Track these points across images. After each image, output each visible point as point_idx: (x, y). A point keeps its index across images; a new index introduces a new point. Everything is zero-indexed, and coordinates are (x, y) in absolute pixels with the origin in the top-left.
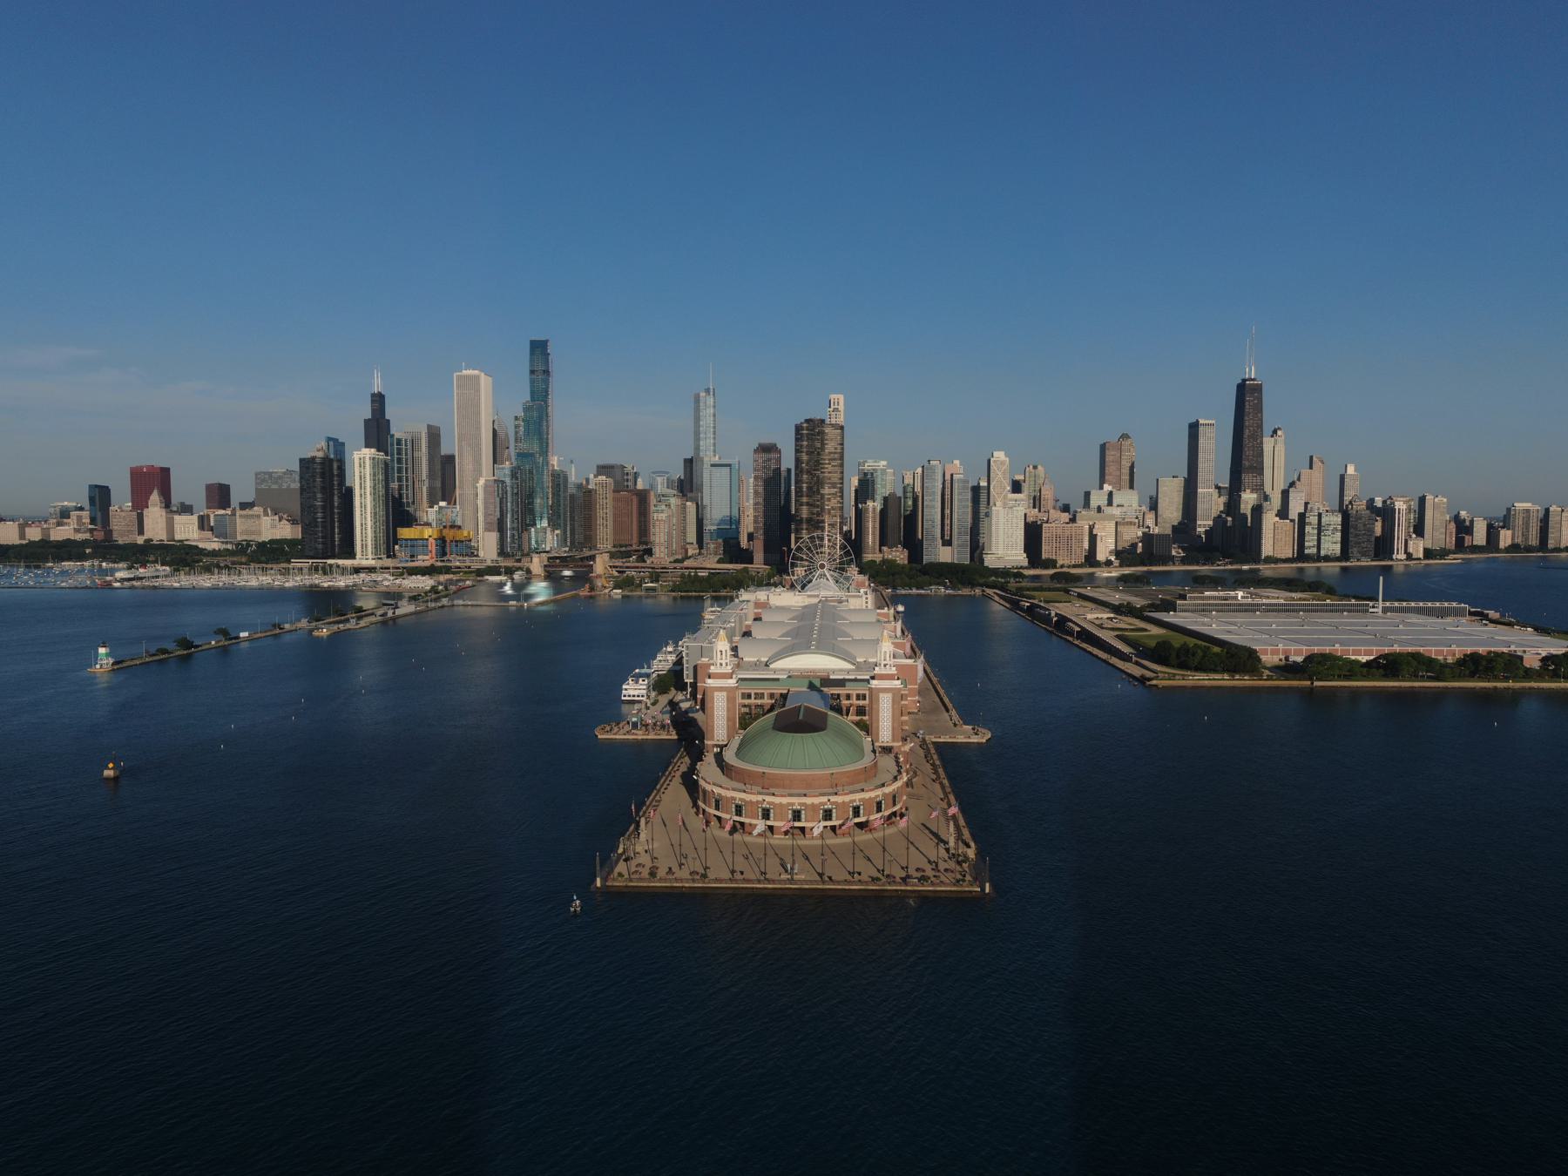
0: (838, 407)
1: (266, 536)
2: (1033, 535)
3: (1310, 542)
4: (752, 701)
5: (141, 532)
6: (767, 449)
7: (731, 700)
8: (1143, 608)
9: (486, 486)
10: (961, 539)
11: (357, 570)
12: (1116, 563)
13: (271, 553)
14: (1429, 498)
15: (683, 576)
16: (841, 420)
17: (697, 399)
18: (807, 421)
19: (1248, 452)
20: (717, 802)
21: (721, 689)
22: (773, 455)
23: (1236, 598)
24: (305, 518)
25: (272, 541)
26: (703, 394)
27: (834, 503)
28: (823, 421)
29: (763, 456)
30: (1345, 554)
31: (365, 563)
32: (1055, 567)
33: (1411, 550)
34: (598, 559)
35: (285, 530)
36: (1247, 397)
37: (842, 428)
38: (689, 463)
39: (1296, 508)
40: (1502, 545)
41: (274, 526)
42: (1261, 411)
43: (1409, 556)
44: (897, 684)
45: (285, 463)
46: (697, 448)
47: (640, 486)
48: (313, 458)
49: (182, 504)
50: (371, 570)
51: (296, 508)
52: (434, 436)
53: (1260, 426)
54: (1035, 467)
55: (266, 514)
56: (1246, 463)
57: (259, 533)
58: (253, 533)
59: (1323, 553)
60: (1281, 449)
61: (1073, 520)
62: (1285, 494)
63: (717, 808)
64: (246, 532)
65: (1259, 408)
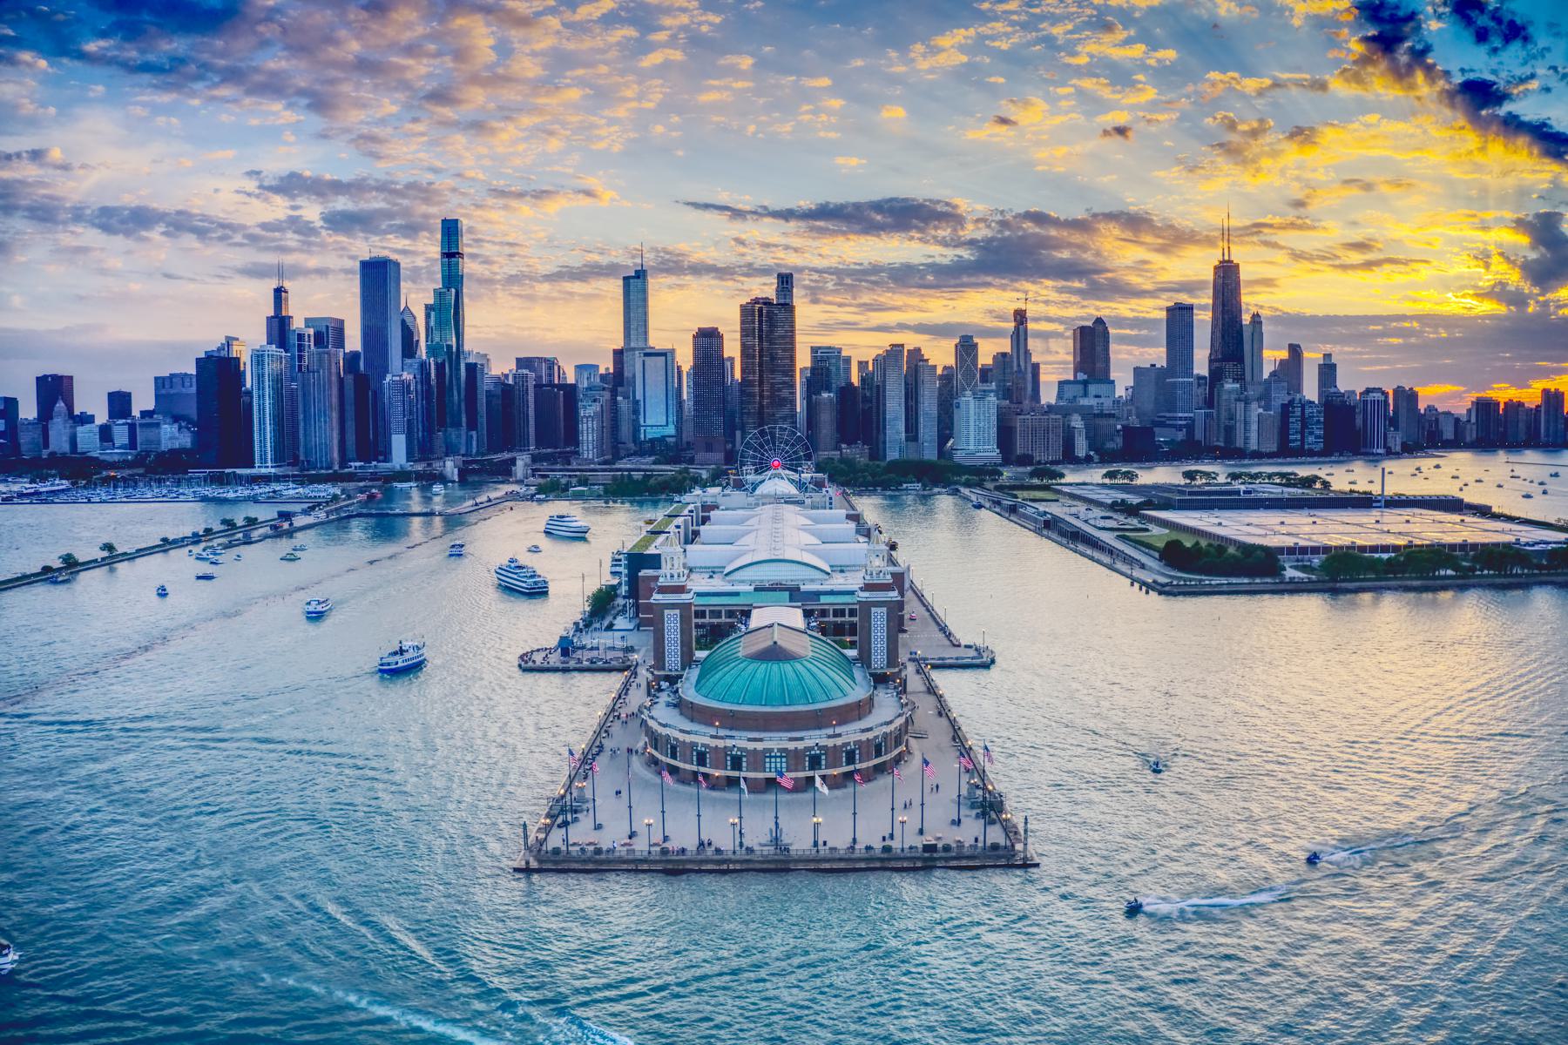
1: (165, 445)
4: (707, 620)
5: (46, 445)
7: (685, 620)
8: (1140, 506)
10: (928, 430)
12: (1096, 458)
15: (614, 478)
20: (674, 748)
21: (673, 606)
24: (202, 427)
25: (172, 451)
28: (1412, 17)
32: (1031, 464)
34: (520, 463)
35: (185, 440)
45: (553, 642)
50: (267, 479)
57: (159, 443)
63: (674, 756)
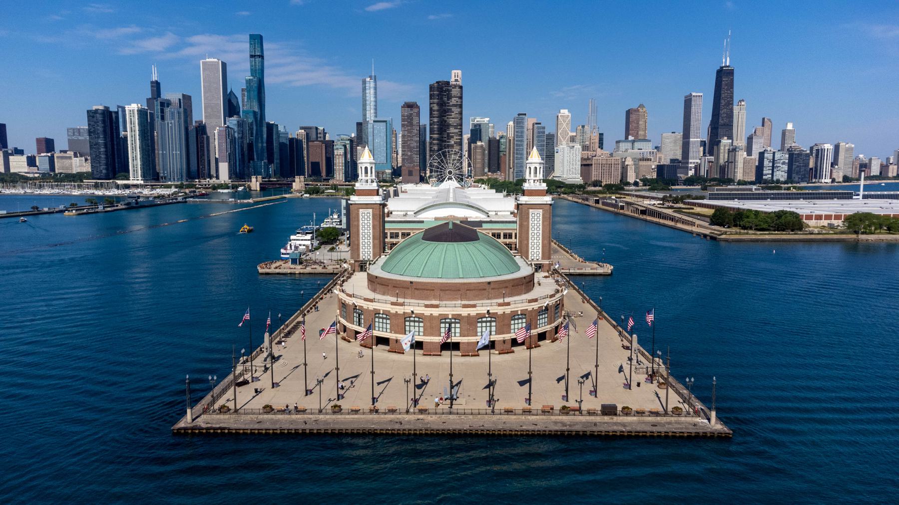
0: (455, 76)
2: (586, 166)
3: (767, 171)
6: (410, 106)
9: (219, 132)
11: (127, 187)
12: (641, 183)
13: (77, 178)
14: (842, 144)
16: (460, 83)
17: (364, 82)
18: (437, 82)
19: (723, 112)
22: (415, 110)
23: (751, 190)
26: (368, 79)
27: (456, 149)
28: (448, 83)
29: (407, 111)
30: (790, 179)
31: (135, 182)
33: (834, 176)
35: (87, 168)
36: (724, 78)
37: (461, 87)
38: (359, 125)
39: (756, 149)
40: (890, 175)
41: (81, 166)
42: (732, 88)
43: (833, 181)
44: (548, 199)
46: (365, 115)
47: (327, 138)
48: (97, 110)
49: (16, 149)
50: (136, 186)
51: (87, 149)
52: (186, 101)
53: (732, 97)
54: (583, 127)
55: (76, 156)
56: (721, 122)
58: (67, 168)
59: (775, 179)
60: (744, 112)
61: (416, 402)
62: (750, 140)
64: (63, 168)
65: (731, 85)
